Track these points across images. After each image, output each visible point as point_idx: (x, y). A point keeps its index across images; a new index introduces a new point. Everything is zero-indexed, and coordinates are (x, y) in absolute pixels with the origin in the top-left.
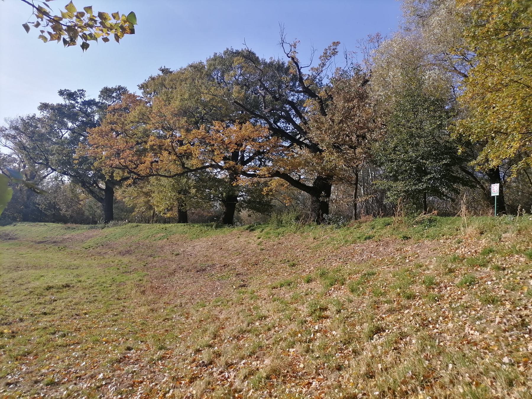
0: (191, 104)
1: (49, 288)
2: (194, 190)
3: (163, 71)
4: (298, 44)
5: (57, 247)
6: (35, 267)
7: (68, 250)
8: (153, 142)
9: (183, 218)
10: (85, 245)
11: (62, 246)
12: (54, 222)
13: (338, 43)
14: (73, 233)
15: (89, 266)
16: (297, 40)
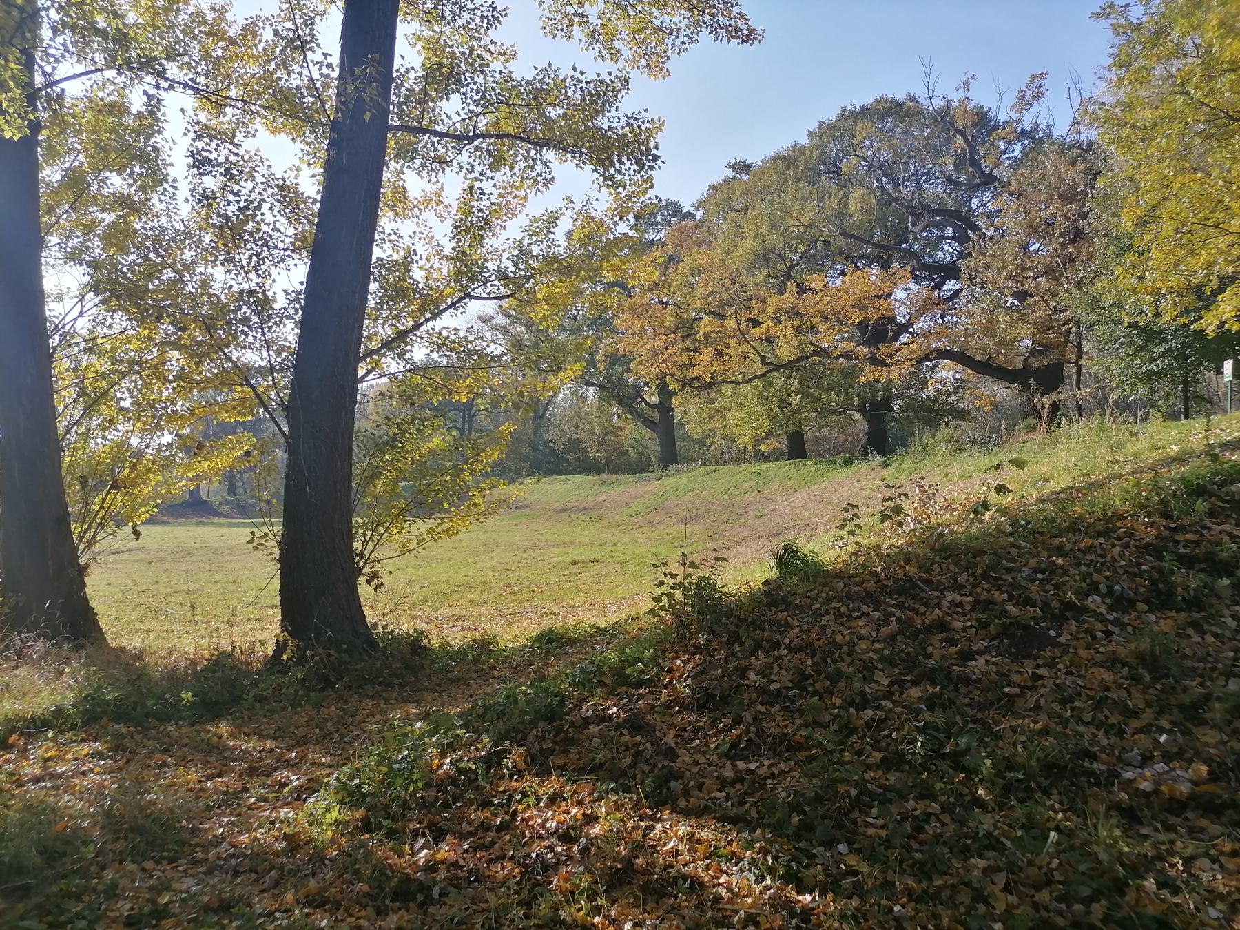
0: (774, 240)
1: (574, 563)
2: (797, 398)
3: (733, 167)
4: (972, 82)
5: (587, 518)
6: (557, 545)
7: (606, 521)
8: (708, 328)
9: (797, 449)
10: (630, 511)
11: (595, 514)
12: (580, 473)
13: (1043, 75)
14: (612, 492)
15: (633, 541)
16: (969, 75)
